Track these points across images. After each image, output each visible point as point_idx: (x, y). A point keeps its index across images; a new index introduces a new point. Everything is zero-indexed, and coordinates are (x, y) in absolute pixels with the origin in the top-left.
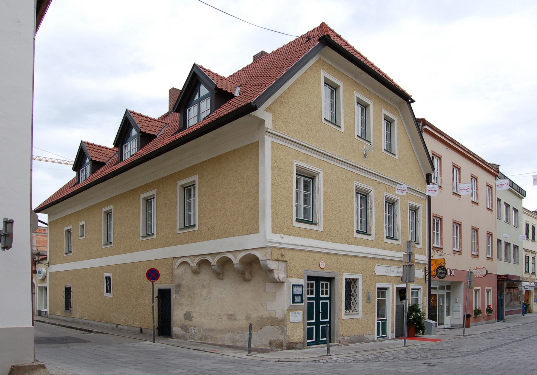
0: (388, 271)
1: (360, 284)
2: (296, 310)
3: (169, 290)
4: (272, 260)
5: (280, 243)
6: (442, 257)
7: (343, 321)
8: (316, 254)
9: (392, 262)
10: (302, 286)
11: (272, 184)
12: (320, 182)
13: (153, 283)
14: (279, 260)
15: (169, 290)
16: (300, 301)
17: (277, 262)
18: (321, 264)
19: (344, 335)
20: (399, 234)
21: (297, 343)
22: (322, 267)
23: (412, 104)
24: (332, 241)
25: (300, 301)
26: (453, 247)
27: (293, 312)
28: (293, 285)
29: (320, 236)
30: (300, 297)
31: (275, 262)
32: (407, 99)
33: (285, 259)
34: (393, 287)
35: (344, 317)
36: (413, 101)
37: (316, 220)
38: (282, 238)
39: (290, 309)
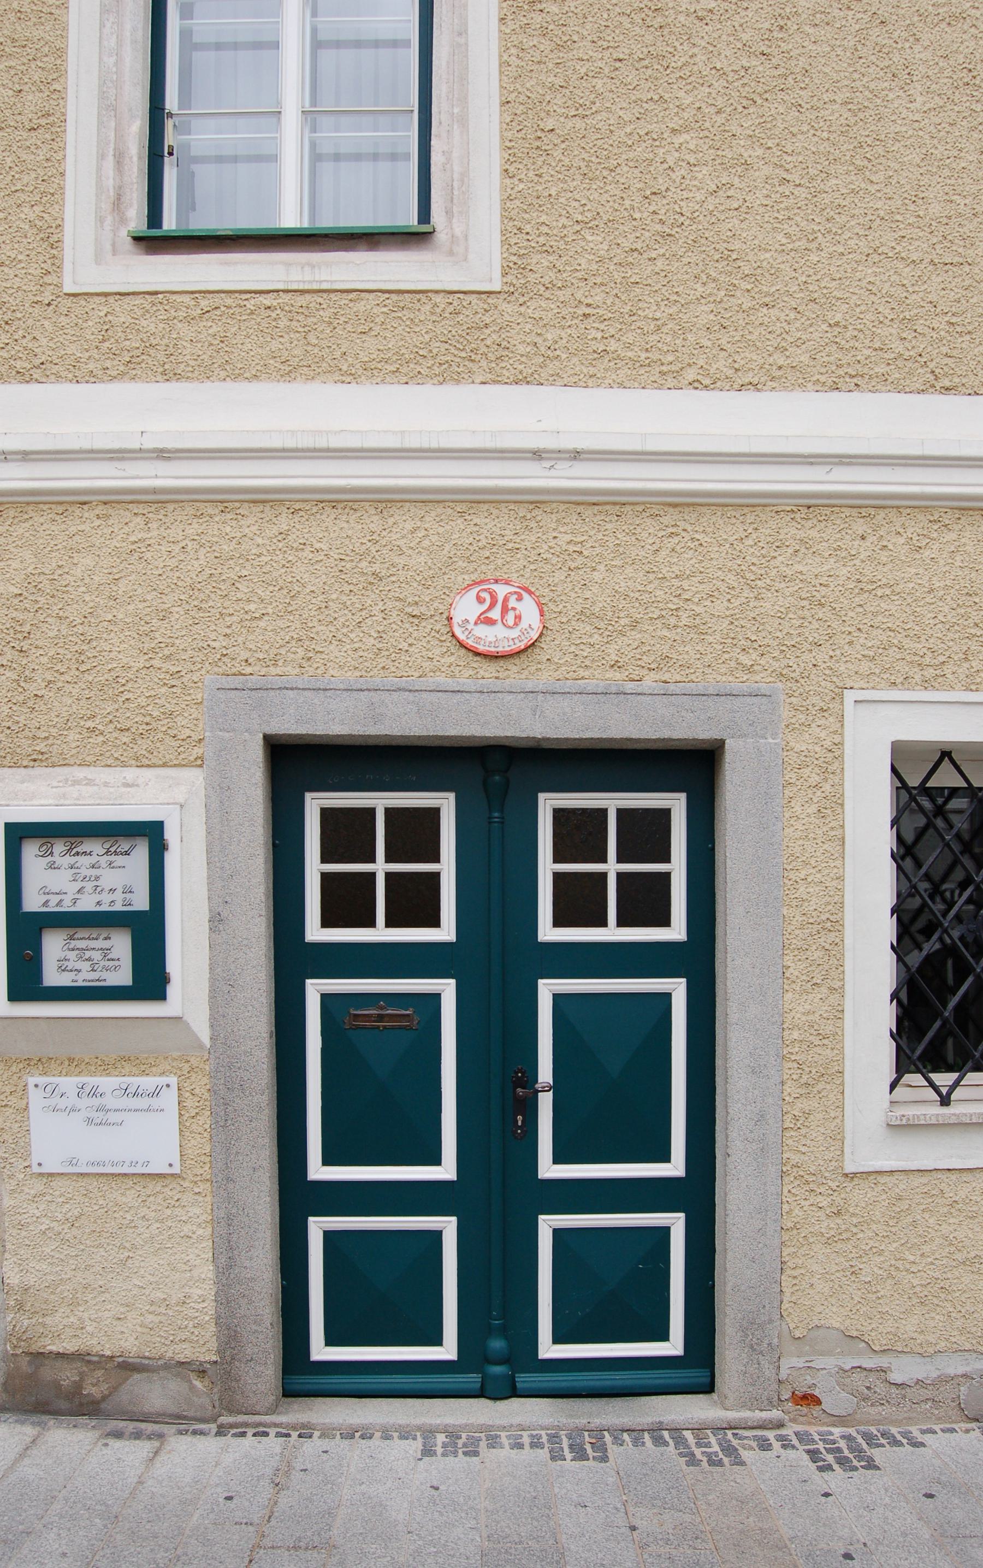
2: (107, 1068)
7: (859, 1195)
10: (152, 834)
16: (123, 976)
18: (466, 608)
21: (129, 1367)
27: (69, 1083)
30: (121, 945)
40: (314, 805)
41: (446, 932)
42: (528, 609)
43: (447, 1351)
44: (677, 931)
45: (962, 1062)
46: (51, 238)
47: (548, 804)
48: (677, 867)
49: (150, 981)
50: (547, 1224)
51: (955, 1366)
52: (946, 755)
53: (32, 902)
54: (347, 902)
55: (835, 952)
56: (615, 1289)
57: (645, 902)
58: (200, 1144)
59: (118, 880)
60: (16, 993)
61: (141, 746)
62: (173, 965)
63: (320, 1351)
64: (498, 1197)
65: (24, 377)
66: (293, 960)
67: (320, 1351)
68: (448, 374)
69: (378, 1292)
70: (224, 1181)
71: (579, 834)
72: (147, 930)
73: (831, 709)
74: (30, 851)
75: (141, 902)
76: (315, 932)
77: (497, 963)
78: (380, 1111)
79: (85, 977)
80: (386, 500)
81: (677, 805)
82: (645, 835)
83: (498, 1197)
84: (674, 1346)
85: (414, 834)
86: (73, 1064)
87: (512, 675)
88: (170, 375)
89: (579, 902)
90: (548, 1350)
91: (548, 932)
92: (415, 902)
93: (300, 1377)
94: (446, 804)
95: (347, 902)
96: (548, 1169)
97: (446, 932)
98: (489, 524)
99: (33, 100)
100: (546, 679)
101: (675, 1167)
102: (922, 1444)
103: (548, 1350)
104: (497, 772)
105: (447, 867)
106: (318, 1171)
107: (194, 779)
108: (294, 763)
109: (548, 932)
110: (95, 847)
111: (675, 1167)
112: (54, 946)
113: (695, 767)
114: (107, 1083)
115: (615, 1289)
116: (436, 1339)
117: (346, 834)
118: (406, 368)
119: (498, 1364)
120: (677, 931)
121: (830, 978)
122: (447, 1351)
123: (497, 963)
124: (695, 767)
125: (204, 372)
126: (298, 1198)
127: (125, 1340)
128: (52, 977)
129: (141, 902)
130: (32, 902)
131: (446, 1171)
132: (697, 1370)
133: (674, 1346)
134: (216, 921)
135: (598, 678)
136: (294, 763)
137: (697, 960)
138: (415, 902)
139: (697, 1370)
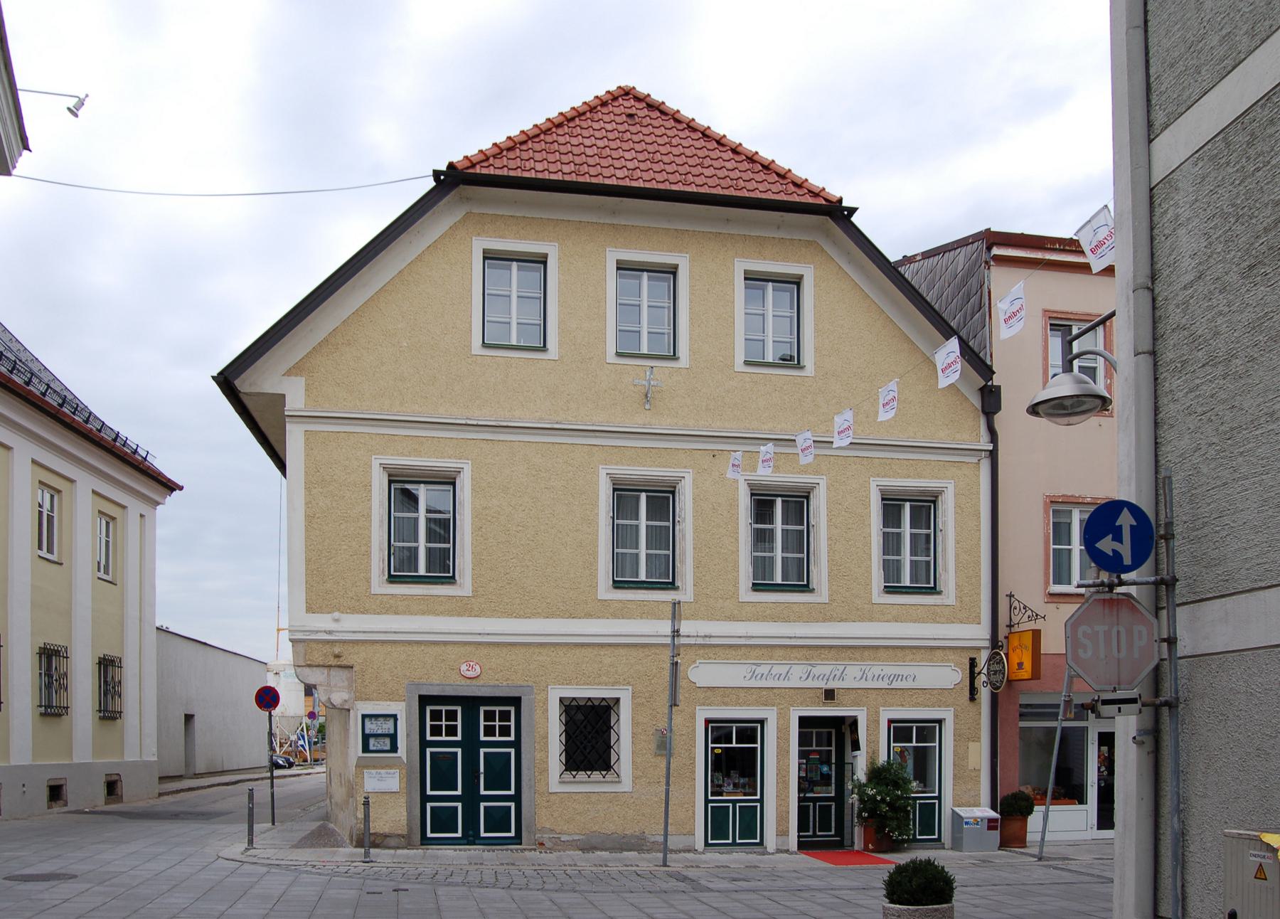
0: (864, 676)
1: (625, 711)
2: (382, 768)
3: (1100, 734)
4: (309, 666)
5: (330, 632)
6: (1032, 626)
7: (553, 798)
8: (450, 648)
9: (795, 653)
10: (395, 717)
11: (307, 516)
12: (820, 507)
13: (270, 716)
14: (330, 666)
15: (1100, 734)
16: (388, 748)
17: (326, 671)
18: (464, 667)
19: (558, 829)
20: (948, 578)
21: (386, 836)
22: (469, 674)
23: (854, 219)
24: (510, 615)
25: (388, 748)
26: (1047, 583)
27: (374, 771)
28: (364, 717)
29: (462, 608)
30: (388, 741)
31: (318, 671)
32: (838, 213)
33: (345, 663)
34: (783, 717)
35: (555, 786)
36: (852, 211)
37: (814, 584)
38: (337, 620)
39: (361, 765)
40: (428, 709)
41: (459, 738)
42: (477, 668)
43: (459, 835)
44: (512, 738)
45: (578, 769)
46: (368, 581)
47: (482, 709)
48: (512, 723)
49: (394, 748)
50: (482, 805)
51: (576, 838)
52: (574, 699)
53: (367, 731)
54: (436, 731)
55: (546, 744)
56: (498, 820)
57: (505, 731)
58: (404, 785)
59: (387, 727)
60: (364, 751)
61: (391, 697)
62: (399, 745)
63: (429, 835)
64: (471, 799)
65: (363, 613)
66: (424, 744)
67: (429, 835)
68: (459, 615)
69: (443, 821)
70: (409, 793)
71: (490, 716)
72: (393, 738)
73: (545, 690)
74: (367, 720)
75: (392, 731)
76: (429, 738)
77: (471, 744)
78: (443, 776)
79: (379, 748)
80: (445, 643)
81: (512, 709)
82: (505, 716)
83: (471, 799)
84: (512, 834)
85: (452, 716)
86: (375, 767)
87: (474, 682)
88: (396, 613)
89: (490, 731)
90: (483, 834)
91: (482, 738)
92: (452, 731)
93: (425, 841)
94: (459, 709)
95: (436, 731)
96: (483, 792)
97: (459, 738)
98: (468, 648)
99: (363, 548)
100: (482, 682)
101: (512, 792)
102: (107, 666)
103: (483, 834)
104: (471, 704)
105: (459, 723)
106: (429, 792)
107: (403, 704)
108: (424, 700)
109: (482, 738)
110: (381, 719)
111: (512, 792)
112: (372, 741)
113: (516, 702)
114: (383, 771)
115: (498, 820)
116: (509, 831)
117: (436, 716)
118: (450, 613)
119: (471, 837)
120: (512, 738)
121: (545, 748)
122: (459, 835)
123: (471, 744)
124: (516, 702)
125: (404, 613)
126: (425, 799)
127: (386, 830)
128: (372, 748)
129: (392, 731)
130: (367, 731)
131: (459, 792)
132: (518, 839)
133: (512, 834)
134: (408, 735)
135: (492, 683)
136: (424, 700)
137: (517, 744)
138: (452, 731)
139: (518, 839)
